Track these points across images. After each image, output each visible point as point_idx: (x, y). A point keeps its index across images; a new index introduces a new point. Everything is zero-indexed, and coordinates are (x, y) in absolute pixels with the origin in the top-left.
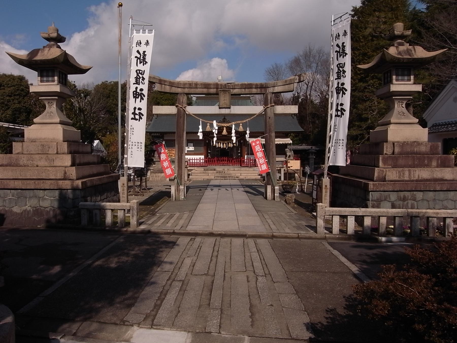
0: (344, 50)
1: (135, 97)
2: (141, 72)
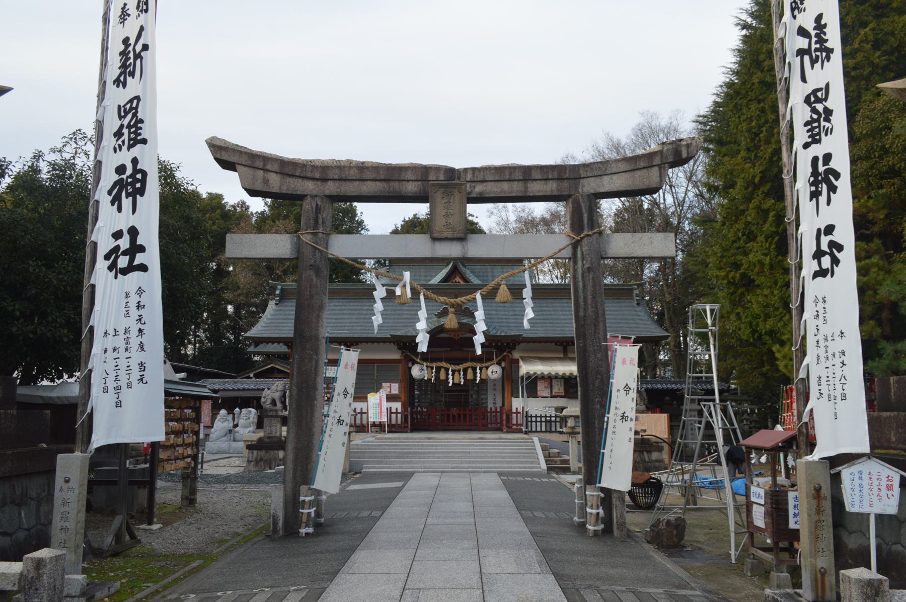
0: (821, 41)
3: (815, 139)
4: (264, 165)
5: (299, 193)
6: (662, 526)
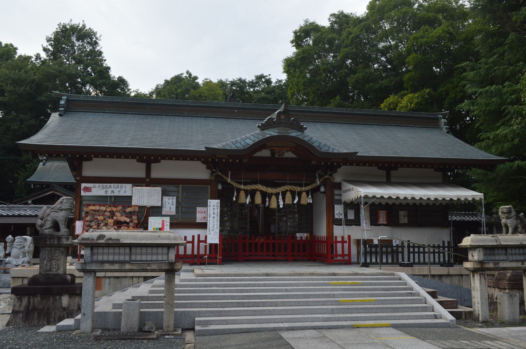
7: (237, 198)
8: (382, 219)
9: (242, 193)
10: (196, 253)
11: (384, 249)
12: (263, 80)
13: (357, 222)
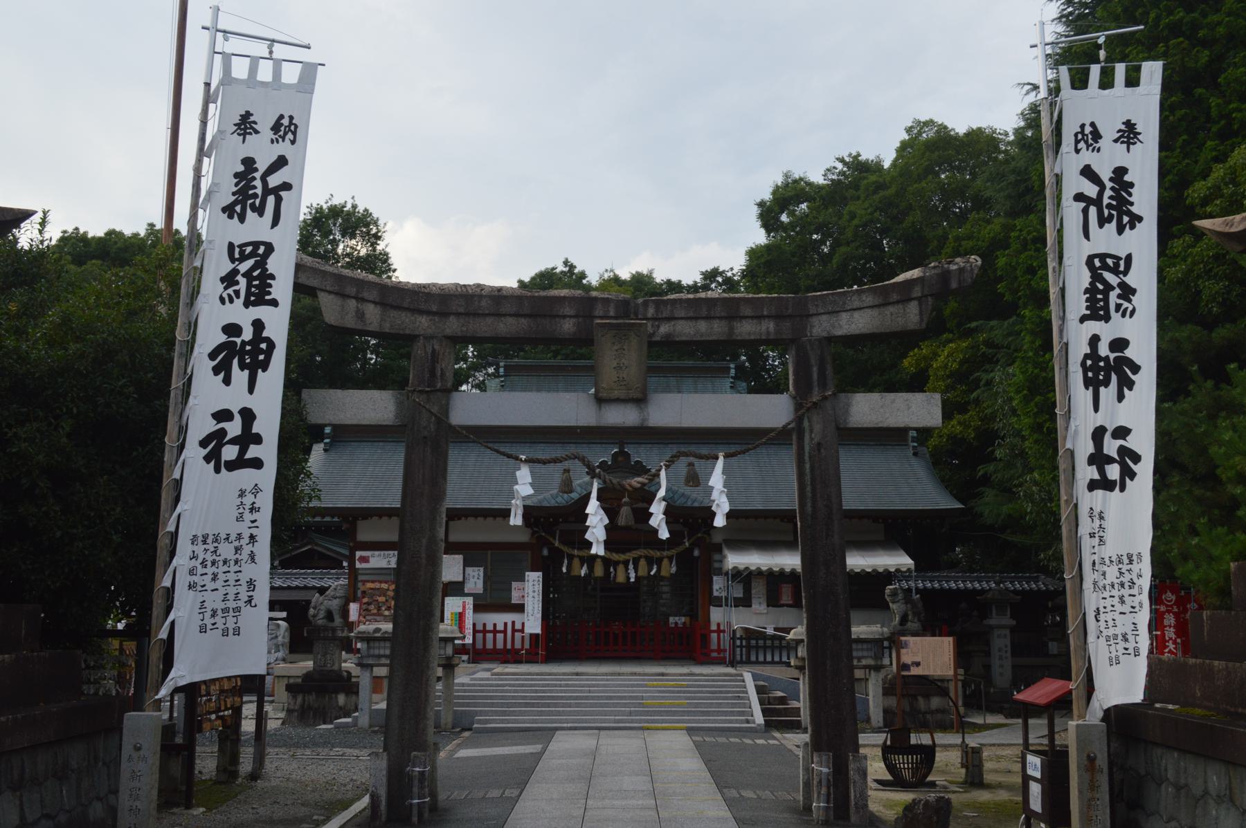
1: (1094, 383)
2: (1110, 262)
3: (1097, 310)
4: (358, 292)
5: (407, 332)
6: (920, 809)
7: (569, 567)
8: (786, 598)
9: (576, 562)
10: (509, 646)
11: (753, 642)
12: (720, 279)
13: (745, 602)
